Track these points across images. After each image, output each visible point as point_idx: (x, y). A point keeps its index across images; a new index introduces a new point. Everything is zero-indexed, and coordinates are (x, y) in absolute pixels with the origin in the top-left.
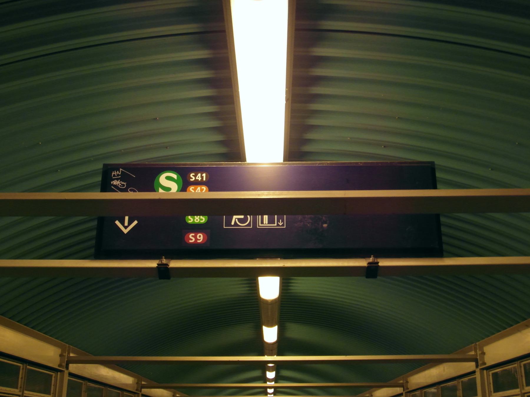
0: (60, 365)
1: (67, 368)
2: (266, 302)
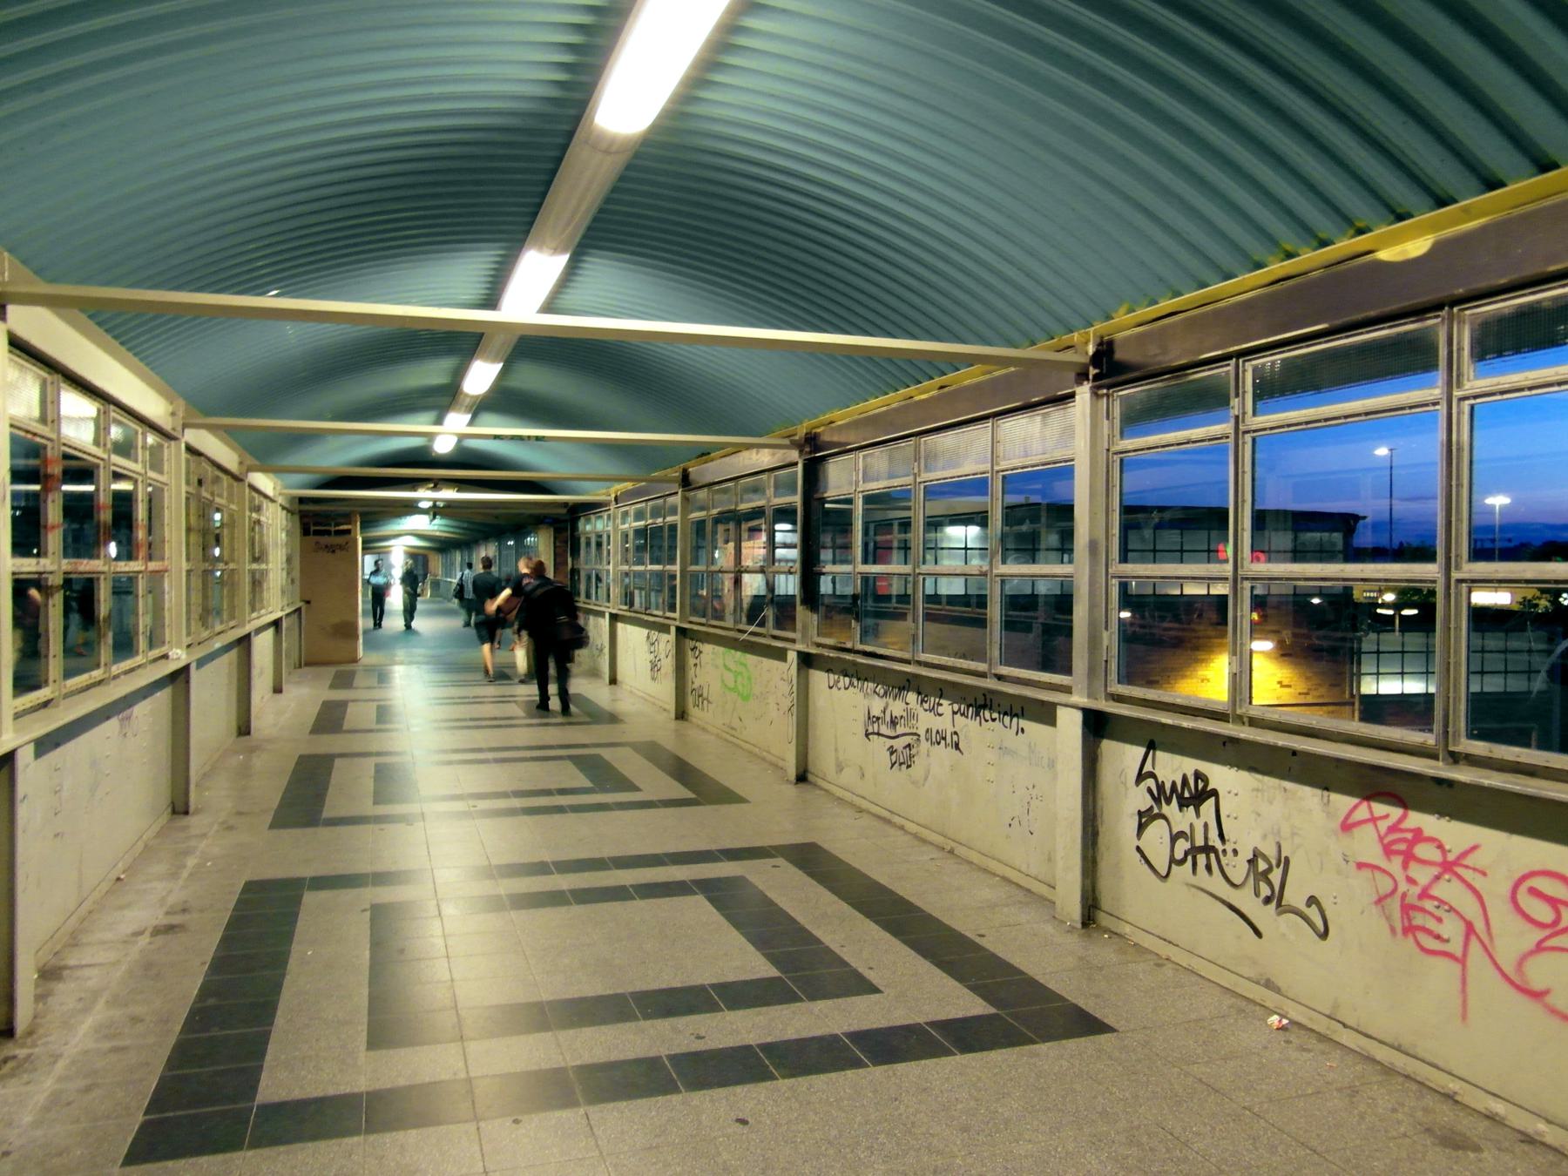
0: (174, 429)
1: (183, 435)
2: (467, 395)
